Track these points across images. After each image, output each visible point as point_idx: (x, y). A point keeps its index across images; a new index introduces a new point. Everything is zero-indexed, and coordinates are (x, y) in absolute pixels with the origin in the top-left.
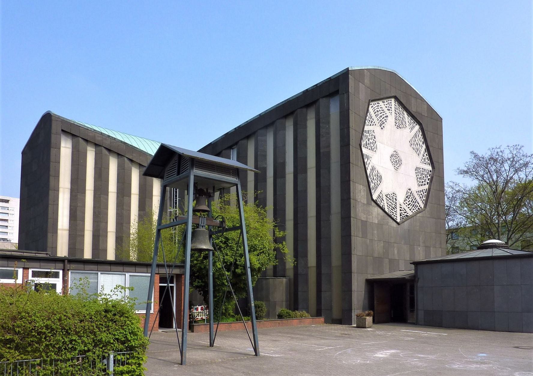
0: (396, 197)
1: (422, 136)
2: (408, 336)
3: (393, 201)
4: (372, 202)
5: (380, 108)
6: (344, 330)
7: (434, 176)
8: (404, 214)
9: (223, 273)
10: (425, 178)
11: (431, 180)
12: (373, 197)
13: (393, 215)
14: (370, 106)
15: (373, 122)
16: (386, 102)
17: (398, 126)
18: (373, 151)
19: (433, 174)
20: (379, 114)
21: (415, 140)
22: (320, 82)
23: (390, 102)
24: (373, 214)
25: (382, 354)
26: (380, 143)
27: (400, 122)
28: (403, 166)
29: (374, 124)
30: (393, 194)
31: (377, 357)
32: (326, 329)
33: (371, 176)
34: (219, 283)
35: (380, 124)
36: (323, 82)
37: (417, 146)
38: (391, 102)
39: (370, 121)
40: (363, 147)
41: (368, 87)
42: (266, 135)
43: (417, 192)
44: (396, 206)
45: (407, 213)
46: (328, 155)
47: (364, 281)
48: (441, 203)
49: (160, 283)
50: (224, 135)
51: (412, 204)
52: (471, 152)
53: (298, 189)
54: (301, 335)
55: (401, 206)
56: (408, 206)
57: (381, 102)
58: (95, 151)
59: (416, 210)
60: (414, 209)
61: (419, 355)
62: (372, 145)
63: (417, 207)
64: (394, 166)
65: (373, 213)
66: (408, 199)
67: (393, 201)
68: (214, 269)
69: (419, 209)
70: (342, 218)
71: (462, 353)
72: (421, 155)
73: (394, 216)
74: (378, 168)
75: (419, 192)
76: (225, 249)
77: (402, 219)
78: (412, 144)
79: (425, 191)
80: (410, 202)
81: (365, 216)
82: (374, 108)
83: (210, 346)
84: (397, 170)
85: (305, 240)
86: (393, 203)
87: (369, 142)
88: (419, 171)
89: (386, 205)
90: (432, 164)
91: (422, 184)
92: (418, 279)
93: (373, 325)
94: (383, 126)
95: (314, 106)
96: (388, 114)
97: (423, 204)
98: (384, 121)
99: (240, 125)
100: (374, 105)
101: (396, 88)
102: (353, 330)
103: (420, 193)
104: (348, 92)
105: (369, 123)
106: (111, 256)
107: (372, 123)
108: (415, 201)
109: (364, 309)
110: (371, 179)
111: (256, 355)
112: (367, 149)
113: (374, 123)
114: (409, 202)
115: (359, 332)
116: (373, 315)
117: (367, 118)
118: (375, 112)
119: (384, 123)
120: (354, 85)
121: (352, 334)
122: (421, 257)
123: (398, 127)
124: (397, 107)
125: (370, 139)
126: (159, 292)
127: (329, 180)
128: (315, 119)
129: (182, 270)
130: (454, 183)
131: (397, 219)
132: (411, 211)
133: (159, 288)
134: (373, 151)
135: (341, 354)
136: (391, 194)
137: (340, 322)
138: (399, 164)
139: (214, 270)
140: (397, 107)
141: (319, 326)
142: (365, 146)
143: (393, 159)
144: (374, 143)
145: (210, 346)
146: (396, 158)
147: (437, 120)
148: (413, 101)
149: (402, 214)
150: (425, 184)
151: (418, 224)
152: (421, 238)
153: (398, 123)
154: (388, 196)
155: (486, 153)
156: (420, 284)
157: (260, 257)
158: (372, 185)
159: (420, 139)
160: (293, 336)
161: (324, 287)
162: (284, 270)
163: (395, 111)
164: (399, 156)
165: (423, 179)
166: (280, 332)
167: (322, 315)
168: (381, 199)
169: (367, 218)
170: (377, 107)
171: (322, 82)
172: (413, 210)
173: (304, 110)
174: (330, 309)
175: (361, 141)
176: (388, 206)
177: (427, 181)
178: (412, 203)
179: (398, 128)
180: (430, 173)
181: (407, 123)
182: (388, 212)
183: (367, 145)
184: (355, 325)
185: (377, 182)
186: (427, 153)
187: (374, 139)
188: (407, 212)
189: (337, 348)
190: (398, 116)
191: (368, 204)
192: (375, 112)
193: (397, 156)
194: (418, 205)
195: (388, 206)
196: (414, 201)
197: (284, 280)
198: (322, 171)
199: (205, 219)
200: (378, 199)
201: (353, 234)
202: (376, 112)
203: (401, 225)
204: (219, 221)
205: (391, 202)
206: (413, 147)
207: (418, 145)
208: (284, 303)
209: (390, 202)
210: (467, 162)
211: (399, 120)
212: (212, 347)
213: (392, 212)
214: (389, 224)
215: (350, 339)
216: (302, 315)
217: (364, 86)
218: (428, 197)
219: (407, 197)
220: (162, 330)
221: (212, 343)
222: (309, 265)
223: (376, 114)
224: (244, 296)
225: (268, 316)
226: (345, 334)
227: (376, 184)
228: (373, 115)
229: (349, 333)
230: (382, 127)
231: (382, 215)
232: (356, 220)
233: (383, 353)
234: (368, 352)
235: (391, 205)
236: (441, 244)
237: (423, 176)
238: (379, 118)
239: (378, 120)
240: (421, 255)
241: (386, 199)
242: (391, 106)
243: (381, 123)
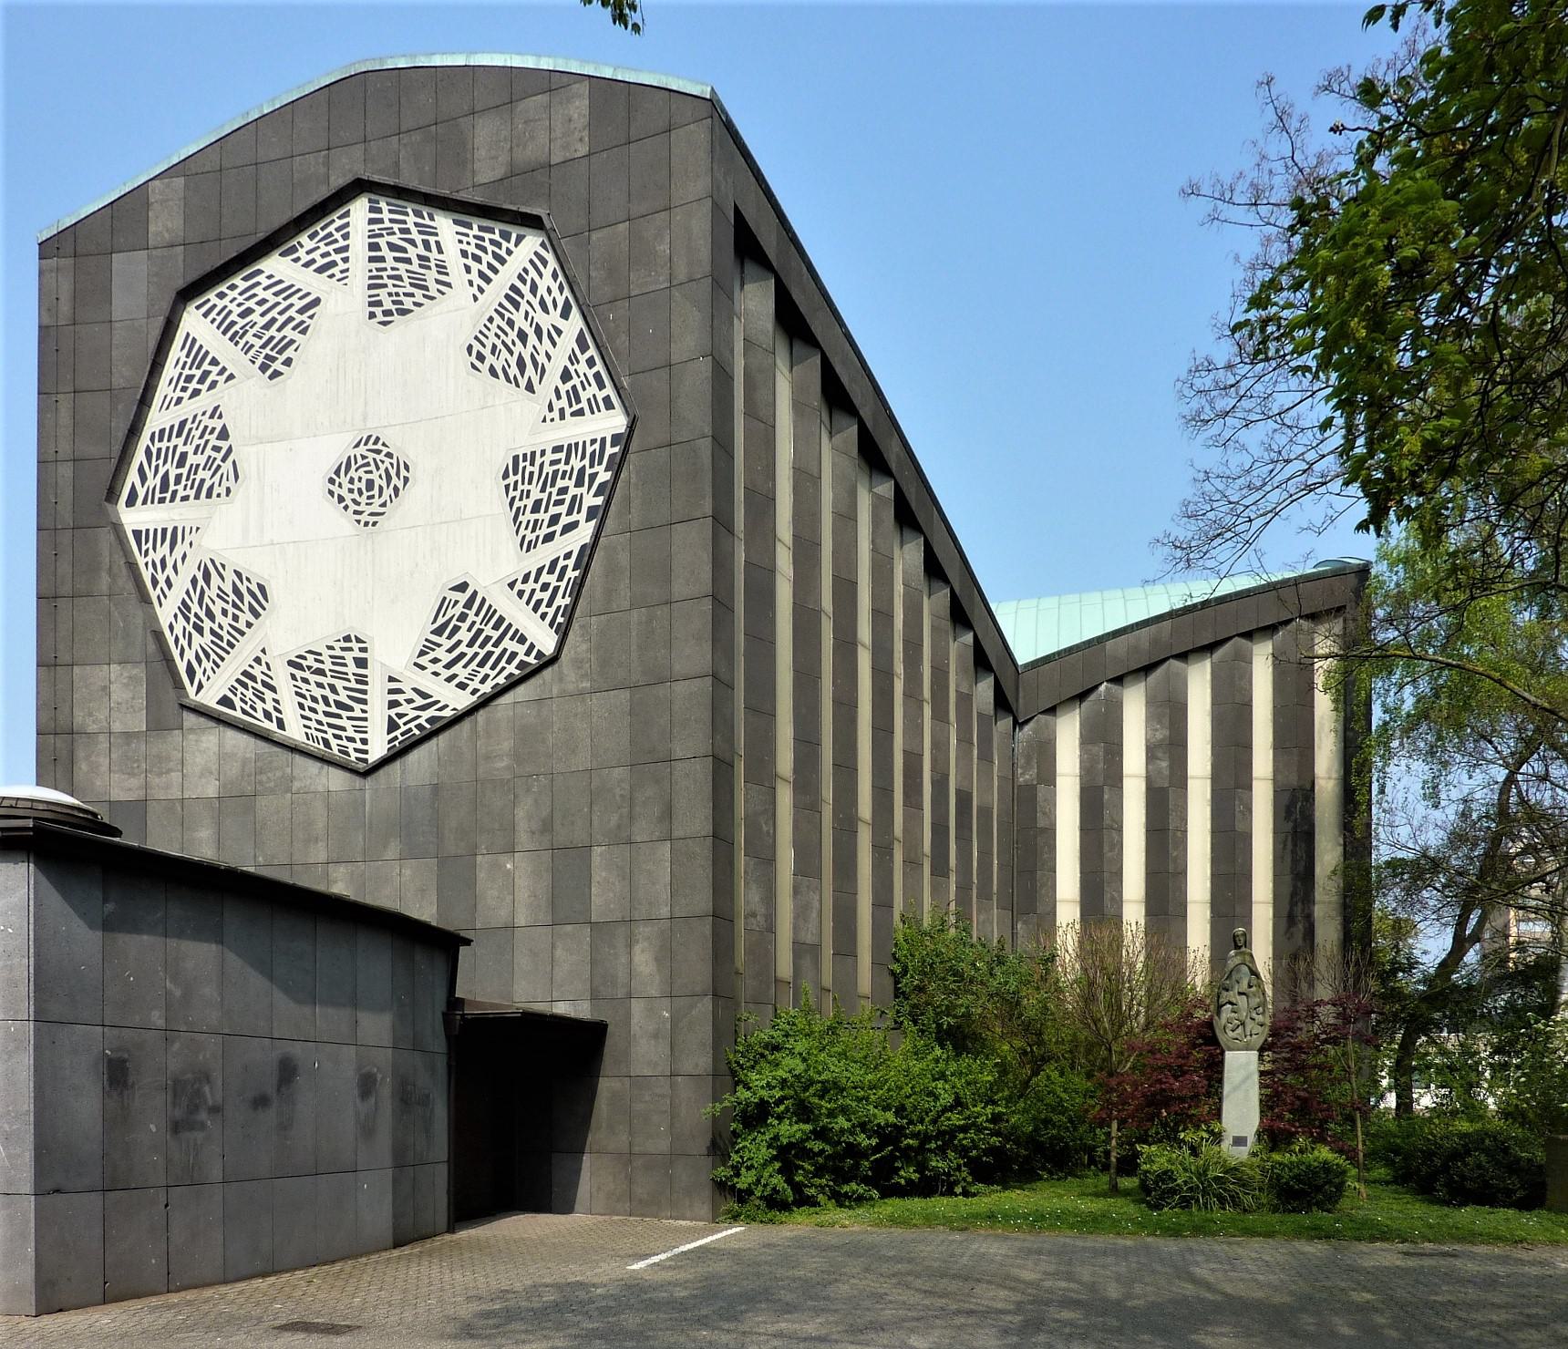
4: (185, 713)
107: (381, 451)
152: (520, 813)
169: (146, 786)
237: (560, 483)
240: (523, 895)
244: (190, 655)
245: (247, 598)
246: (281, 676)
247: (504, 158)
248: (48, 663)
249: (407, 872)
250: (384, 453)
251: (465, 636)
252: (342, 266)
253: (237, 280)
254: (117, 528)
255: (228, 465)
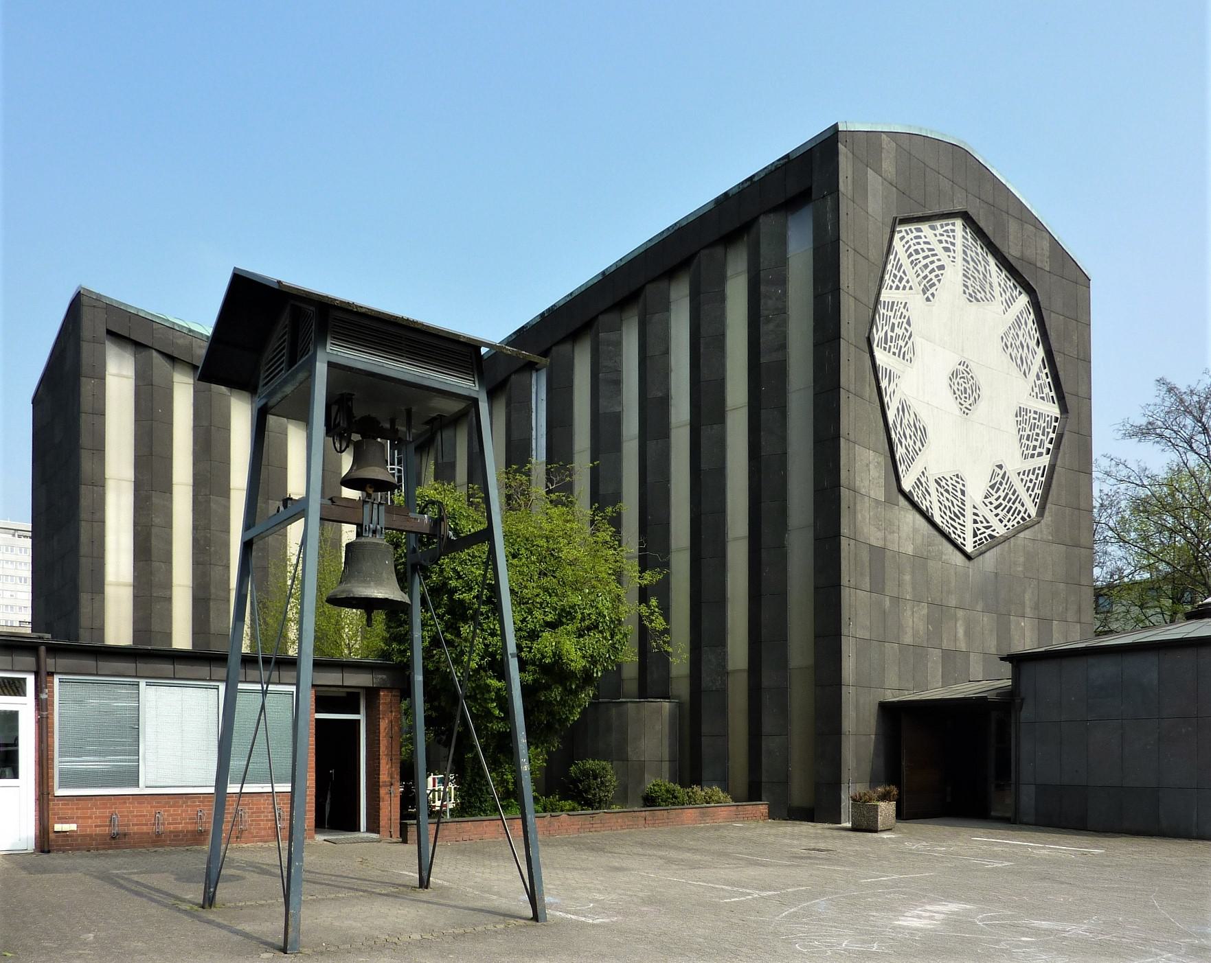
0: (964, 485)
1: (1035, 325)
2: (995, 856)
3: (955, 497)
5: (925, 243)
6: (816, 837)
7: (1066, 432)
8: (985, 532)
9: (486, 684)
10: (1041, 437)
11: (1058, 442)
12: (902, 482)
13: (954, 533)
14: (897, 237)
15: (905, 279)
16: (939, 227)
17: (970, 295)
18: (904, 358)
19: (1063, 427)
20: (921, 259)
21: (1017, 334)
22: (761, 171)
23: (950, 227)
24: (901, 529)
25: (919, 917)
26: (923, 338)
27: (978, 283)
28: (982, 406)
29: (908, 286)
30: (955, 478)
31: (904, 928)
32: (769, 835)
33: (898, 426)
34: (478, 710)
35: (922, 286)
36: (770, 168)
37: (1020, 350)
38: (953, 228)
39: (895, 276)
40: (878, 346)
41: (891, 184)
42: (619, 329)
43: (1019, 474)
44: (964, 510)
45: (994, 530)
46: (781, 369)
47: (874, 709)
48: (1083, 505)
49: (316, 712)
50: (514, 333)
51: (1006, 506)
52: (1158, 381)
53: (702, 466)
54: (695, 851)
55: (975, 511)
56: (995, 512)
57: (925, 227)
58: (194, 384)
59: (1015, 523)
60: (1010, 519)
61: (1037, 923)
62: (901, 343)
63: (1018, 515)
64: (960, 403)
65: (901, 526)
66: (996, 492)
67: (955, 497)
68: (462, 674)
69: (1023, 519)
70: (816, 539)
71: (1168, 916)
72: (1032, 376)
73: (957, 537)
74: (916, 406)
75: (1024, 475)
76: (488, 618)
77: (979, 545)
78: (1009, 345)
79: (1041, 472)
80: (1001, 500)
81: (880, 535)
82: (907, 242)
83: (421, 886)
84: (967, 414)
85: (721, 601)
86: (955, 502)
87: (894, 335)
88: (1025, 417)
89: (936, 506)
90: (1061, 399)
91: (1034, 452)
92: (1023, 700)
93: (899, 825)
94: (930, 292)
95: (745, 239)
96: (945, 261)
97: (1035, 505)
98: (935, 280)
99: (554, 305)
100: (908, 234)
101: (966, 190)
102: (841, 838)
103: (1028, 476)
104: (834, 189)
105: (893, 282)
106: (182, 639)
107: (901, 283)
108: (1013, 498)
109: (874, 783)
110: (898, 435)
111: (536, 918)
112: (889, 352)
113: (906, 284)
114: (997, 500)
115: (857, 844)
116: (896, 797)
117: (889, 267)
118: (909, 252)
119: (934, 285)
120: (853, 173)
121: (839, 851)
122: (1026, 641)
123: (973, 298)
124: (970, 244)
125: (896, 325)
126: (316, 735)
127: (783, 439)
128: (747, 275)
129: (380, 676)
130: (1112, 459)
131: (965, 546)
132: (1004, 524)
133: (314, 723)
134: (904, 358)
135: (794, 915)
136: (951, 479)
137: (807, 815)
138: (972, 399)
139: (459, 675)
140: (970, 244)
141: (754, 825)
142: (883, 345)
143: (956, 384)
144: (907, 339)
145: (421, 886)
146: (966, 381)
147: (1076, 283)
148: (1013, 226)
149: (978, 532)
150: (1040, 454)
151: (1022, 560)
152: (1027, 596)
153: (971, 288)
154: (943, 484)
155: (1199, 380)
156: (1026, 714)
157: (586, 640)
158: (900, 452)
159: (1029, 332)
160: (673, 854)
161: (768, 724)
162: (666, 679)
163: (965, 252)
164: (972, 377)
165: (1036, 440)
166: (642, 844)
167: (763, 798)
168: (924, 490)
169: (885, 539)
170: (915, 241)
171: (765, 168)
172: (1008, 521)
173: (719, 251)
174: (785, 782)
175: (871, 328)
176: (943, 508)
177: (1047, 445)
178: (1004, 503)
179: (971, 301)
180: (1054, 424)
181: (997, 289)
182: (941, 524)
183: (889, 343)
184: (849, 825)
185: (915, 443)
186: (1047, 370)
187: (907, 327)
188: (991, 526)
189: (787, 894)
190: (972, 269)
191: (889, 501)
192: (909, 252)
193: (969, 377)
194: (1023, 510)
195: (943, 508)
196: (1012, 497)
197: (666, 705)
198: (764, 414)
199: (382, 508)
200: (917, 489)
201: (847, 582)
202: (913, 253)
203: (975, 560)
204: (430, 518)
205: (950, 498)
206: (1011, 355)
207: (1025, 348)
208: (666, 766)
209: (948, 499)
210: (1149, 405)
211: (975, 279)
212: (426, 890)
213: (952, 525)
214: (944, 557)
215: (828, 865)
216: (710, 798)
217: (880, 178)
218: (1047, 487)
219: (992, 487)
220: (326, 838)
221: (425, 878)
222: (730, 667)
223: (912, 258)
224: (554, 746)
225: (623, 798)
226: (818, 850)
227: (910, 450)
228: (905, 262)
229: (830, 847)
230: (928, 294)
231: (925, 533)
232: (855, 545)
233: (924, 914)
234: (877, 910)
235: (949, 508)
236: (1079, 610)
237: (1037, 431)
238: (920, 272)
239: (919, 275)
241: (938, 491)
242: (954, 239)
243: (925, 285)
246: (933, 487)
249: (985, 619)
250: (899, 284)
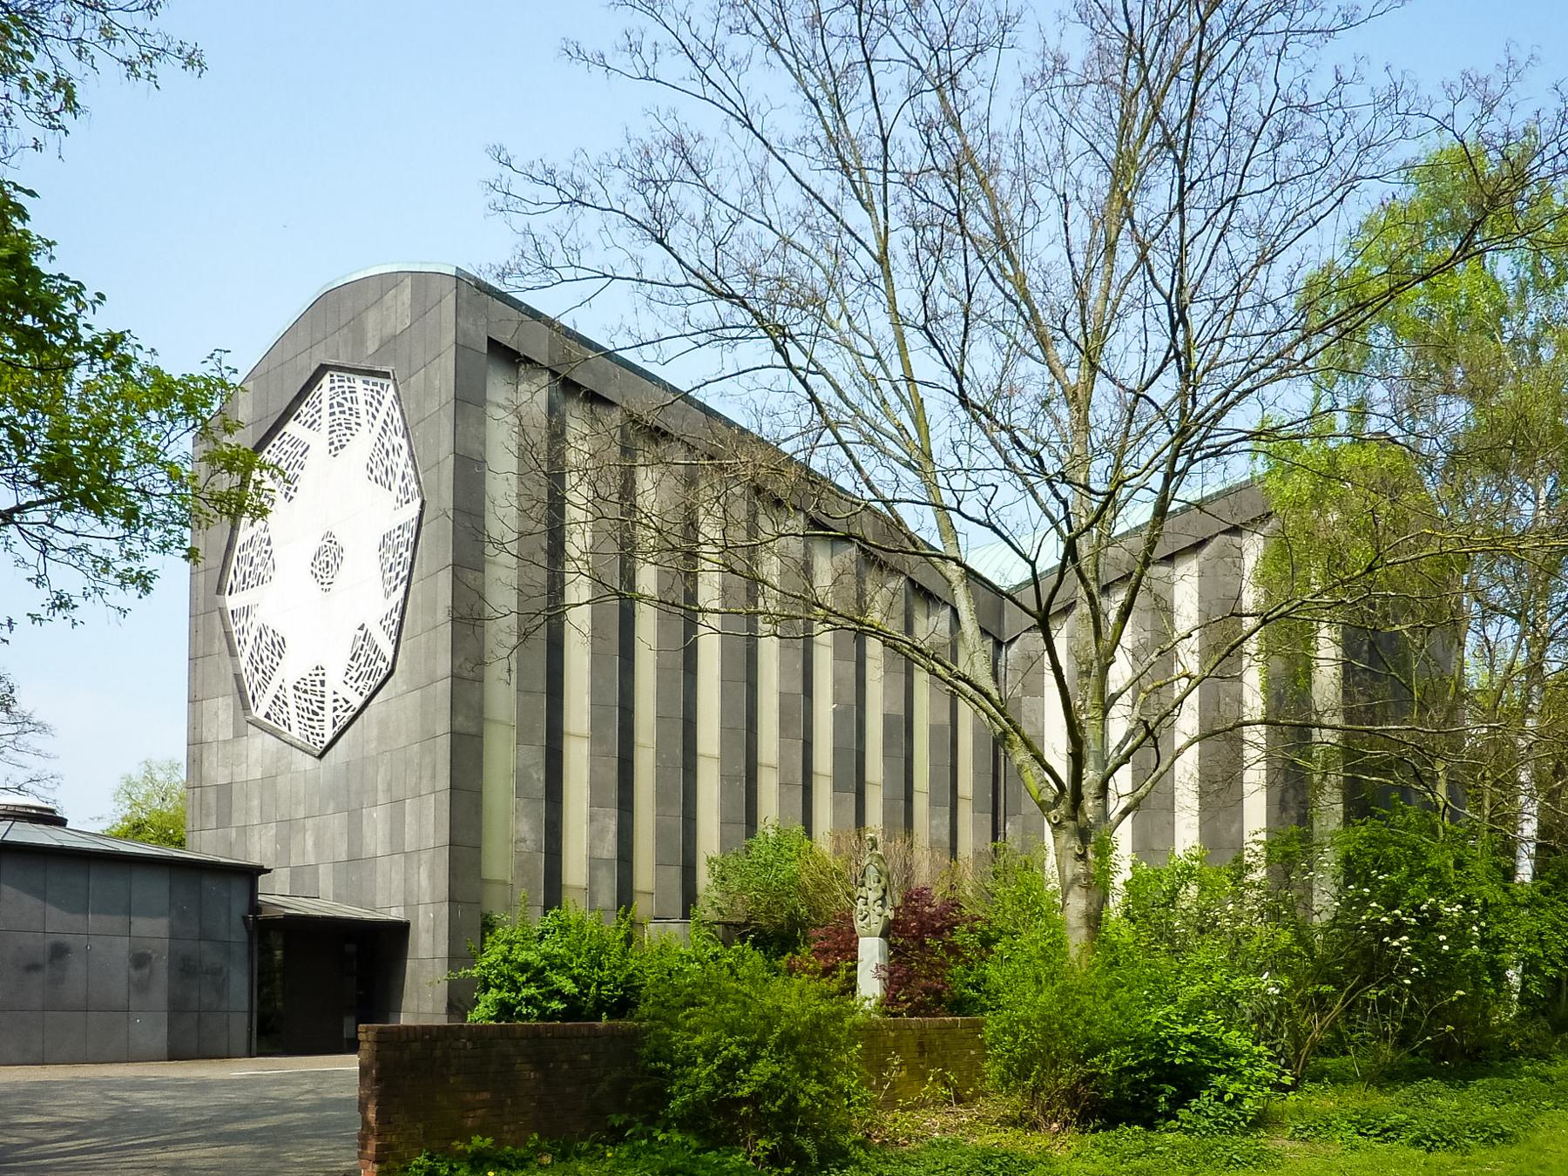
244: (253, 687)
245: (277, 647)
247: (377, 338)
248: (192, 701)
251: (363, 659)
252: (319, 421)
253: (276, 441)
254: (222, 610)
255: (270, 562)
